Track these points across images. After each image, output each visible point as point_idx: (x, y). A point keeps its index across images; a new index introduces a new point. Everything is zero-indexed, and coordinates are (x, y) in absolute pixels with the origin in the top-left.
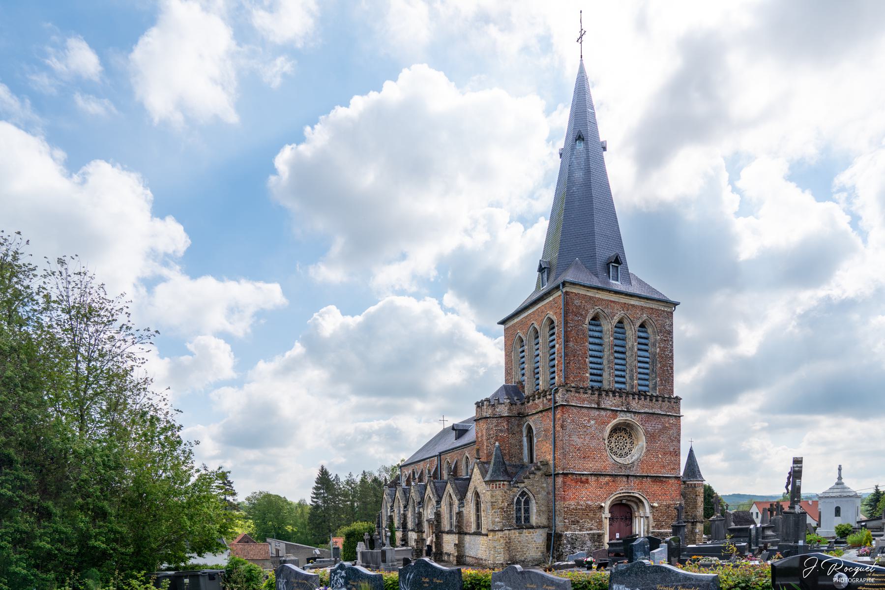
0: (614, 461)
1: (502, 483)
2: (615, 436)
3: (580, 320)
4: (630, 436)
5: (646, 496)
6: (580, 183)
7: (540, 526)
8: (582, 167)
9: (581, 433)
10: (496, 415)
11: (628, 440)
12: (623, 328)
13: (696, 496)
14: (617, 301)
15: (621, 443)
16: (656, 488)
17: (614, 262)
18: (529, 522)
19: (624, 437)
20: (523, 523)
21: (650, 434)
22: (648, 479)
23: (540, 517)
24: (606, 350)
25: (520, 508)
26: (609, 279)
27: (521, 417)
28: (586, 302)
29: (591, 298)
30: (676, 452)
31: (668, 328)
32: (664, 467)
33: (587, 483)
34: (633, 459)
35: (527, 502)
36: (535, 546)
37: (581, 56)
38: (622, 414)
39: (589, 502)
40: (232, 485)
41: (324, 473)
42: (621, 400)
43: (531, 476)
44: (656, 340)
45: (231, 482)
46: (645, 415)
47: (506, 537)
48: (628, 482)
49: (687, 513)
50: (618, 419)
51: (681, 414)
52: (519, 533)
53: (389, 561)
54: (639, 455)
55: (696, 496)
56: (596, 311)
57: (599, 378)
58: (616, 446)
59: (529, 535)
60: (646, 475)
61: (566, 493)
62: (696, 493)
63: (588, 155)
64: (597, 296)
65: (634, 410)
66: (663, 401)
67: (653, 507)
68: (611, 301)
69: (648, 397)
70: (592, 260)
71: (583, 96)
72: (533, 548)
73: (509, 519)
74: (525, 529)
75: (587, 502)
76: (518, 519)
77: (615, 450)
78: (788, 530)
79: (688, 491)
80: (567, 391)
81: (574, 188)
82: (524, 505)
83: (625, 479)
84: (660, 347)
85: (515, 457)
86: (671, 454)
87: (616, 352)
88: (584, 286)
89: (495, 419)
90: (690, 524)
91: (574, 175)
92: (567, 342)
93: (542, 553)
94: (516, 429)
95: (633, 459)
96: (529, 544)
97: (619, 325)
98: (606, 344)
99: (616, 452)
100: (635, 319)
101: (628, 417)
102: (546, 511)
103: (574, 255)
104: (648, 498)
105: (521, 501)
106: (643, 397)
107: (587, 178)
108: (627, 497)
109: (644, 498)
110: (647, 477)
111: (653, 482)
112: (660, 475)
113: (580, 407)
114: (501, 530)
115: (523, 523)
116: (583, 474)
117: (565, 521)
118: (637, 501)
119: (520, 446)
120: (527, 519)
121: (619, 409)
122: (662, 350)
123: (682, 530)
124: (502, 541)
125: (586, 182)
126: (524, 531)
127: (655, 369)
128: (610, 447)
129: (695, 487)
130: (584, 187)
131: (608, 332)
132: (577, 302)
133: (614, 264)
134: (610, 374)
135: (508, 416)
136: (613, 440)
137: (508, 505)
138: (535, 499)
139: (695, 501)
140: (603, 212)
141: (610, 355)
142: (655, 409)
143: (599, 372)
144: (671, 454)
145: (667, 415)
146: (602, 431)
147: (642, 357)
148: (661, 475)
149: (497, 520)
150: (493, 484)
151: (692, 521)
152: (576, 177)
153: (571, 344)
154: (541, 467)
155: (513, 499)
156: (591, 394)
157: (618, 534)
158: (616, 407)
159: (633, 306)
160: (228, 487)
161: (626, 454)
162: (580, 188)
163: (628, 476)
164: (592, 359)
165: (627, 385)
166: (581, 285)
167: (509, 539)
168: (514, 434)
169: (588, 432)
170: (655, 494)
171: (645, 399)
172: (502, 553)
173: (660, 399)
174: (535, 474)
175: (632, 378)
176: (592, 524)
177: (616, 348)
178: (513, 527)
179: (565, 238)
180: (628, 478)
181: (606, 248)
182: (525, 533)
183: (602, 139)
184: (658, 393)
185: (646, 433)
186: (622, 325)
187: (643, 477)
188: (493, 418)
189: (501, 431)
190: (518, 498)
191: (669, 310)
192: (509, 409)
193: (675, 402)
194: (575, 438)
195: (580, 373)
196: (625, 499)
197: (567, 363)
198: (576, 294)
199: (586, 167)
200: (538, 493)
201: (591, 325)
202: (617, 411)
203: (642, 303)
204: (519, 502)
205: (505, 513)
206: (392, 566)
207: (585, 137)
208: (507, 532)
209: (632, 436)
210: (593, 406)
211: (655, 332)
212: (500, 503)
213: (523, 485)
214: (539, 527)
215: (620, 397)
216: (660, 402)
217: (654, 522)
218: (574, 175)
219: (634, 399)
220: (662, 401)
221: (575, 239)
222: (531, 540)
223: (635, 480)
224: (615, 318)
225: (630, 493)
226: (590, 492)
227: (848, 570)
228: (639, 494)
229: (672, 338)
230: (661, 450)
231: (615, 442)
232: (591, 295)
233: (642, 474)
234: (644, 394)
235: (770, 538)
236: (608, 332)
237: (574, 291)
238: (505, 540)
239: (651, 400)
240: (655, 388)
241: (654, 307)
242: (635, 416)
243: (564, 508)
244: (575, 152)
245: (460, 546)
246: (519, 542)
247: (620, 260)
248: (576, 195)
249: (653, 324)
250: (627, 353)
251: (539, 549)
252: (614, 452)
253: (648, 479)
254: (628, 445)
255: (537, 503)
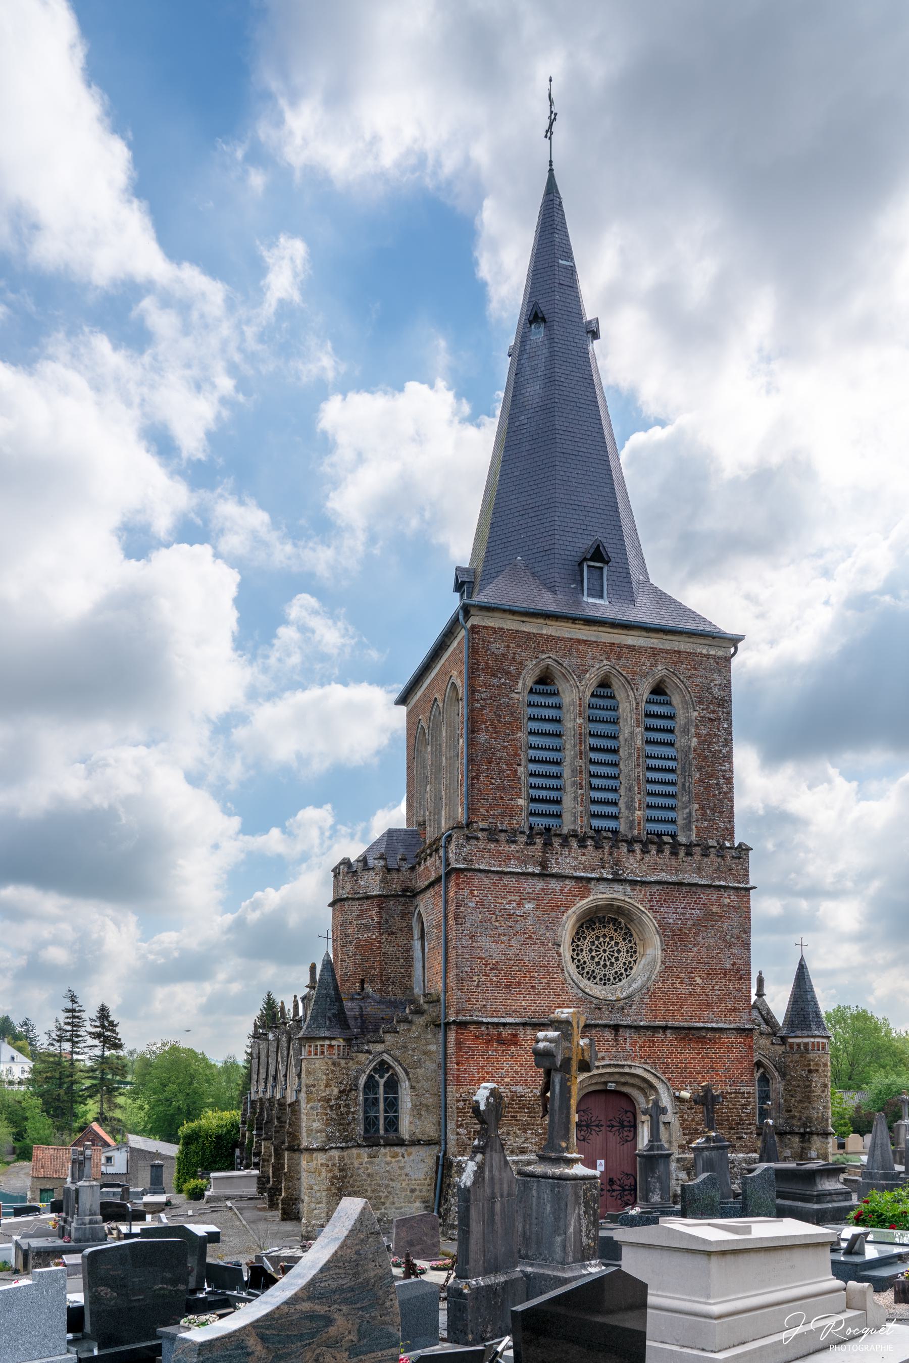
0: (581, 994)
1: (327, 1042)
2: (591, 936)
3: (503, 684)
4: (628, 935)
5: (664, 1073)
6: (534, 406)
7: (419, 1141)
8: (539, 374)
9: (500, 931)
10: (358, 893)
11: (622, 944)
12: (613, 697)
13: (810, 1071)
14: (593, 639)
15: (605, 951)
16: (688, 1054)
17: (591, 559)
18: (396, 1130)
19: (611, 938)
20: (382, 1132)
21: (672, 930)
22: (668, 1033)
23: (420, 1119)
24: (568, 746)
25: (377, 1100)
26: (580, 596)
27: (409, 896)
28: (518, 646)
29: (530, 636)
30: (738, 970)
31: (717, 692)
32: (709, 1005)
33: (516, 1044)
34: (631, 989)
35: (392, 1085)
36: (408, 1185)
37: (551, 162)
38: (602, 886)
39: (519, 1089)
40: (117, 1029)
41: (270, 1004)
42: (599, 854)
43: (402, 1027)
44: (689, 721)
45: (115, 1023)
46: (660, 887)
47: (334, 1165)
48: (616, 1041)
49: (791, 1111)
50: (591, 898)
51: (752, 883)
52: (370, 1156)
53: (84, 1212)
54: (645, 979)
55: (810, 1071)
56: (542, 664)
57: (553, 808)
58: (593, 958)
59: (393, 1160)
60: (663, 1023)
61: (462, 1068)
62: (810, 1065)
63: (551, 350)
64: (544, 632)
65: (631, 877)
66: (705, 855)
67: (679, 1099)
68: (578, 641)
69: (668, 846)
70: (546, 558)
71: (550, 236)
72: (404, 1190)
73: (340, 1124)
74: (385, 1146)
75: (513, 1088)
76: (370, 1123)
77: (590, 966)
78: (528, 1227)
79: (792, 1062)
80: (468, 838)
81: (523, 417)
82: (386, 1092)
83: (608, 1035)
84: (698, 736)
85: (393, 983)
86: (725, 975)
87: (593, 749)
88: (513, 612)
89: (357, 903)
90: (796, 1139)
91: (523, 392)
92: (473, 732)
93: (424, 1202)
94: (398, 923)
95: (631, 989)
96: (392, 1180)
97: (601, 691)
98: (569, 733)
99: (593, 971)
100: (637, 678)
101: (618, 894)
102: (434, 1107)
103: (514, 552)
104: (669, 1079)
105: (378, 1083)
106: (653, 849)
107: (548, 393)
108: (607, 1076)
109: (658, 1078)
110: (665, 1028)
111: (681, 1040)
112: (697, 1025)
113: (498, 872)
114: (322, 1150)
115: (382, 1132)
116: (504, 1025)
117: (460, 1130)
118: (644, 1085)
119: (406, 959)
120: (392, 1124)
121: (593, 875)
122: (706, 741)
123: (662, 1167)
124: (324, 1174)
125: (546, 402)
126: (383, 1150)
127: (687, 784)
128: (579, 961)
129: (807, 1049)
130: (540, 413)
131: (572, 708)
132: (498, 647)
133: (592, 564)
134: (575, 799)
135: (379, 896)
136: (585, 945)
137: (341, 1092)
138: (409, 1079)
139: (807, 1083)
140: (580, 458)
141: (575, 757)
142: (686, 872)
143: (553, 794)
144: (725, 975)
145: (714, 886)
146: (552, 925)
147: (654, 758)
148: (702, 1025)
149: (316, 1125)
150: (310, 1046)
151: (802, 1130)
152: (528, 394)
153: (482, 737)
154: (426, 1007)
155: (357, 1078)
156: (527, 844)
157: (603, 1161)
158: (586, 871)
159: (632, 648)
160: (109, 1033)
161: (619, 977)
162: (533, 415)
163: (616, 1028)
164: (533, 767)
165: (622, 821)
166: (505, 611)
167: (341, 1170)
168: (393, 933)
169: (518, 927)
170: (685, 1069)
171: (660, 851)
172: (324, 1200)
173: (697, 850)
174: (410, 1022)
175: (630, 807)
176: (527, 1139)
177: (593, 742)
178: (355, 1141)
179: (499, 519)
180: (617, 1031)
181: (580, 531)
182: (385, 1155)
183: (589, 316)
184: (694, 838)
185: (663, 927)
186: (609, 691)
187: (655, 1029)
188: (353, 899)
189: (367, 927)
190: (370, 1077)
191: (720, 653)
192: (384, 881)
193: (733, 857)
194: (485, 942)
195: (502, 798)
196: (612, 1079)
197: (473, 778)
198: (495, 630)
199: (547, 372)
200: (418, 1064)
201: (536, 693)
202: (589, 880)
203: (653, 640)
204: (371, 1085)
205: (332, 1110)
206: (90, 1223)
207: (546, 316)
208: (335, 1153)
209: (631, 935)
210: (530, 870)
211: (686, 702)
212: (322, 1088)
213: (380, 1047)
214: (416, 1143)
215: (598, 847)
216: (697, 858)
217: (684, 1134)
218: (523, 392)
219: (631, 851)
220: (703, 855)
221: (518, 518)
222: (399, 1172)
223: (635, 1036)
224: (587, 676)
225: (623, 1066)
226: (521, 1066)
227: (852, 1333)
228: (645, 1069)
229: (729, 713)
230: (701, 966)
231: (591, 951)
232: (531, 631)
233: (652, 1024)
234: (656, 839)
235: (828, 1198)
236: (572, 708)
237: (491, 624)
238: (331, 1171)
239: (674, 853)
240: (687, 827)
241: (682, 647)
242: (634, 890)
243: (458, 1101)
244: (527, 347)
245: (292, 1177)
246: (369, 1175)
247: (604, 553)
248: (525, 431)
249: (682, 686)
250: (621, 750)
251: (417, 1193)
252: (588, 973)
253: (668, 1033)
254: (623, 957)
255: (412, 1087)
